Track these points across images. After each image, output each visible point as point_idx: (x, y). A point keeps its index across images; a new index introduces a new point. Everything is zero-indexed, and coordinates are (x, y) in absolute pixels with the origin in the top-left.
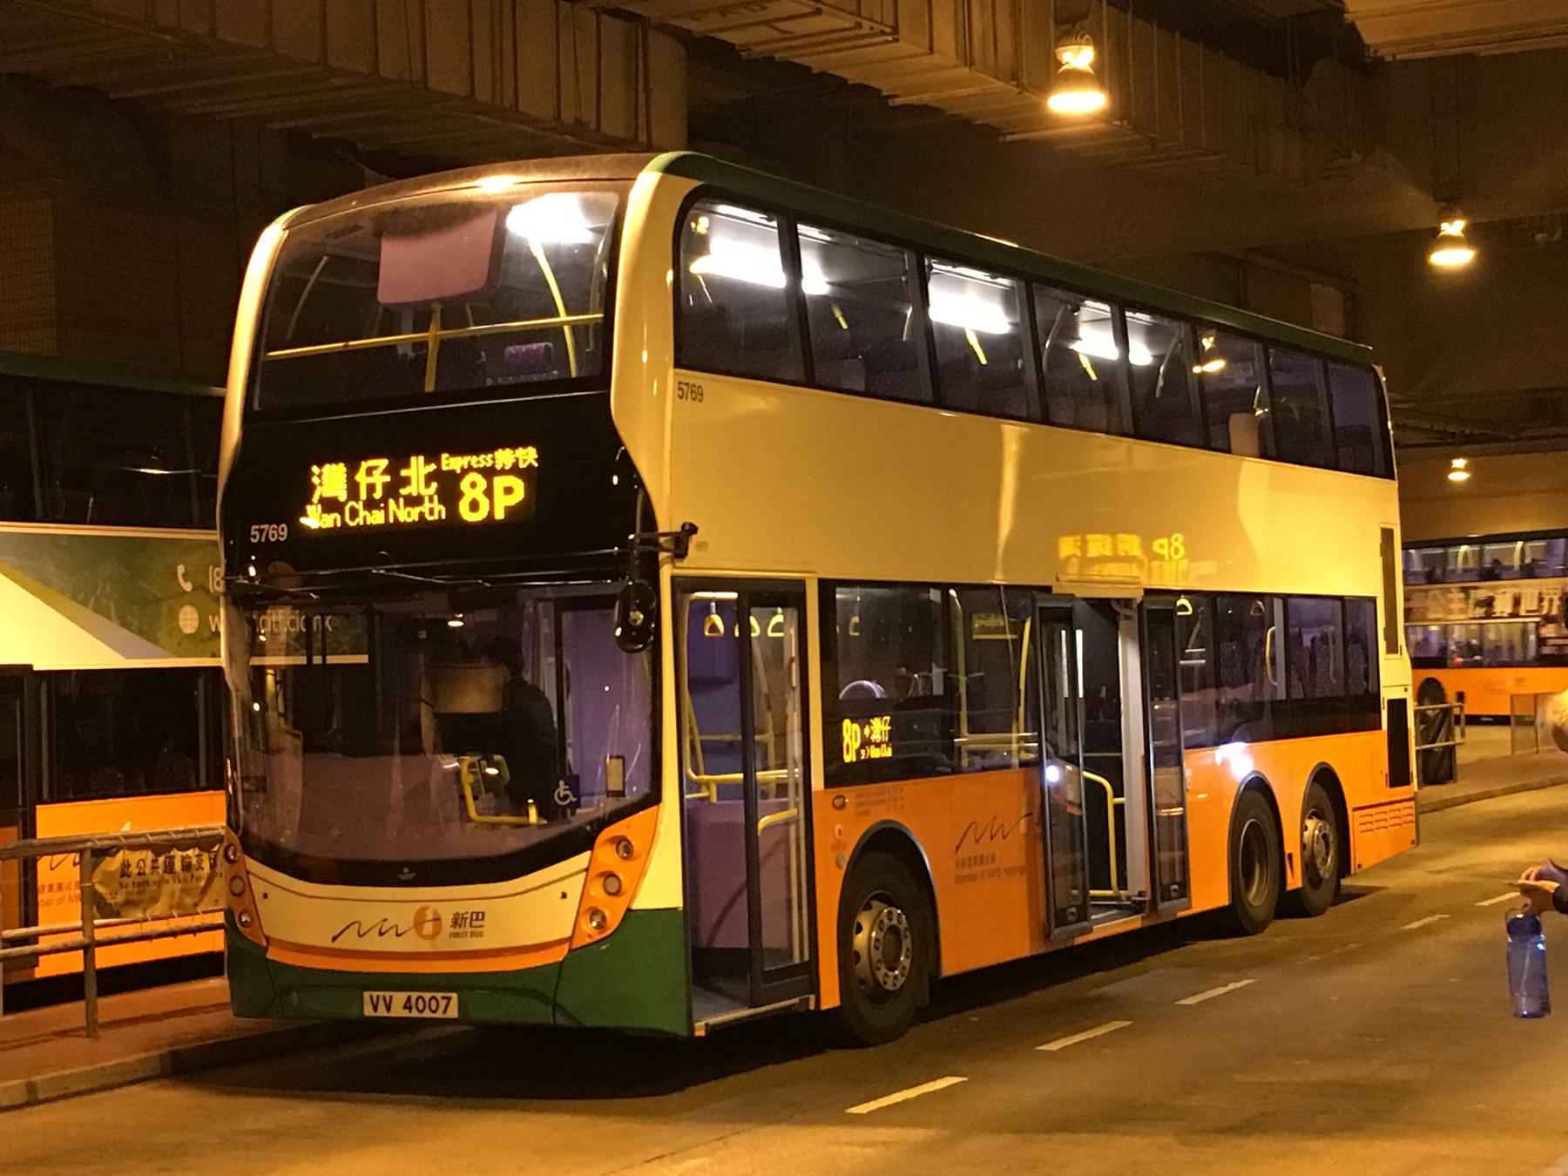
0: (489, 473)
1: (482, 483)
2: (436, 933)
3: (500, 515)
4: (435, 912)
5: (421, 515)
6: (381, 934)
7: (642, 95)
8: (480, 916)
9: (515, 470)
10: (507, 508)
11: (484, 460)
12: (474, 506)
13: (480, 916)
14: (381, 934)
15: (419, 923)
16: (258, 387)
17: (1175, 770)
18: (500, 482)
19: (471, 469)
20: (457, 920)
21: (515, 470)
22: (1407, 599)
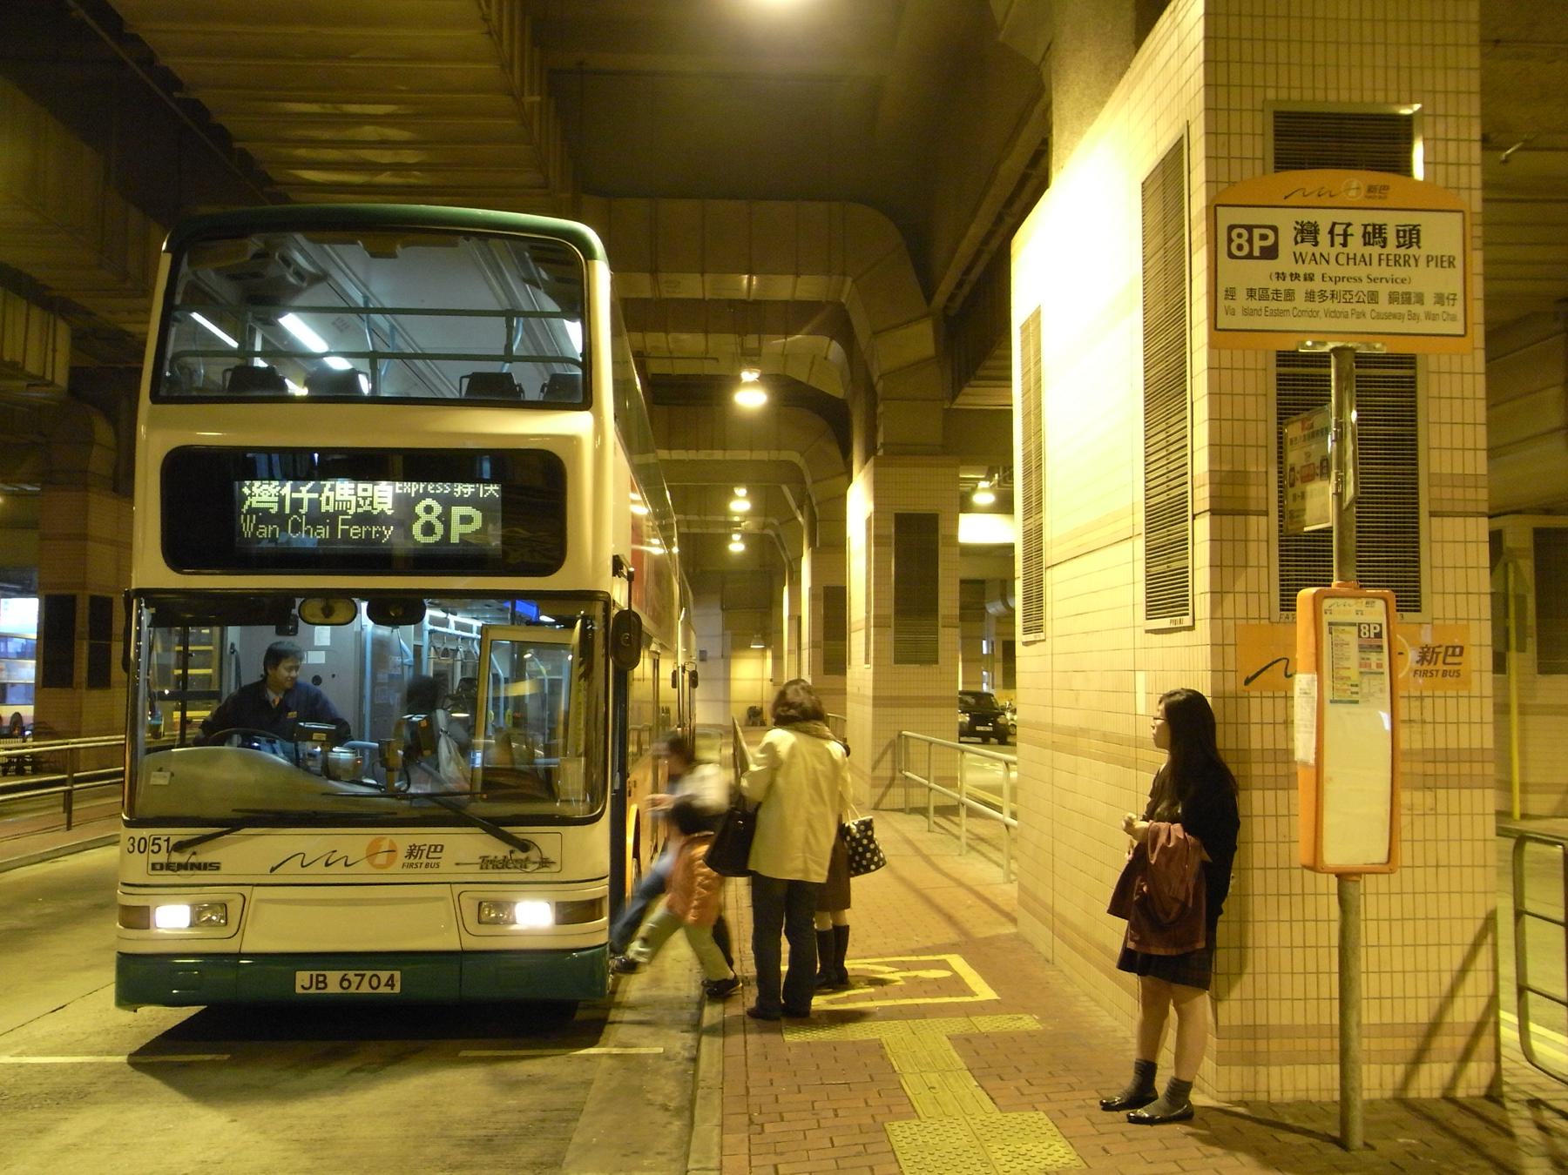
0: (448, 502)
1: (438, 509)
2: (390, 863)
3: (455, 539)
4: (391, 842)
5: (369, 533)
6: (327, 865)
7: (50, 353)
8: (1386, 188)
9: (473, 501)
10: (461, 535)
11: (443, 488)
12: (428, 529)
13: (1386, 188)
14: (327, 865)
15: (371, 855)
16: (249, 394)
17: (1484, 508)
18: (457, 512)
19: (426, 495)
20: (412, 852)
21: (473, 501)
22: (1519, 696)
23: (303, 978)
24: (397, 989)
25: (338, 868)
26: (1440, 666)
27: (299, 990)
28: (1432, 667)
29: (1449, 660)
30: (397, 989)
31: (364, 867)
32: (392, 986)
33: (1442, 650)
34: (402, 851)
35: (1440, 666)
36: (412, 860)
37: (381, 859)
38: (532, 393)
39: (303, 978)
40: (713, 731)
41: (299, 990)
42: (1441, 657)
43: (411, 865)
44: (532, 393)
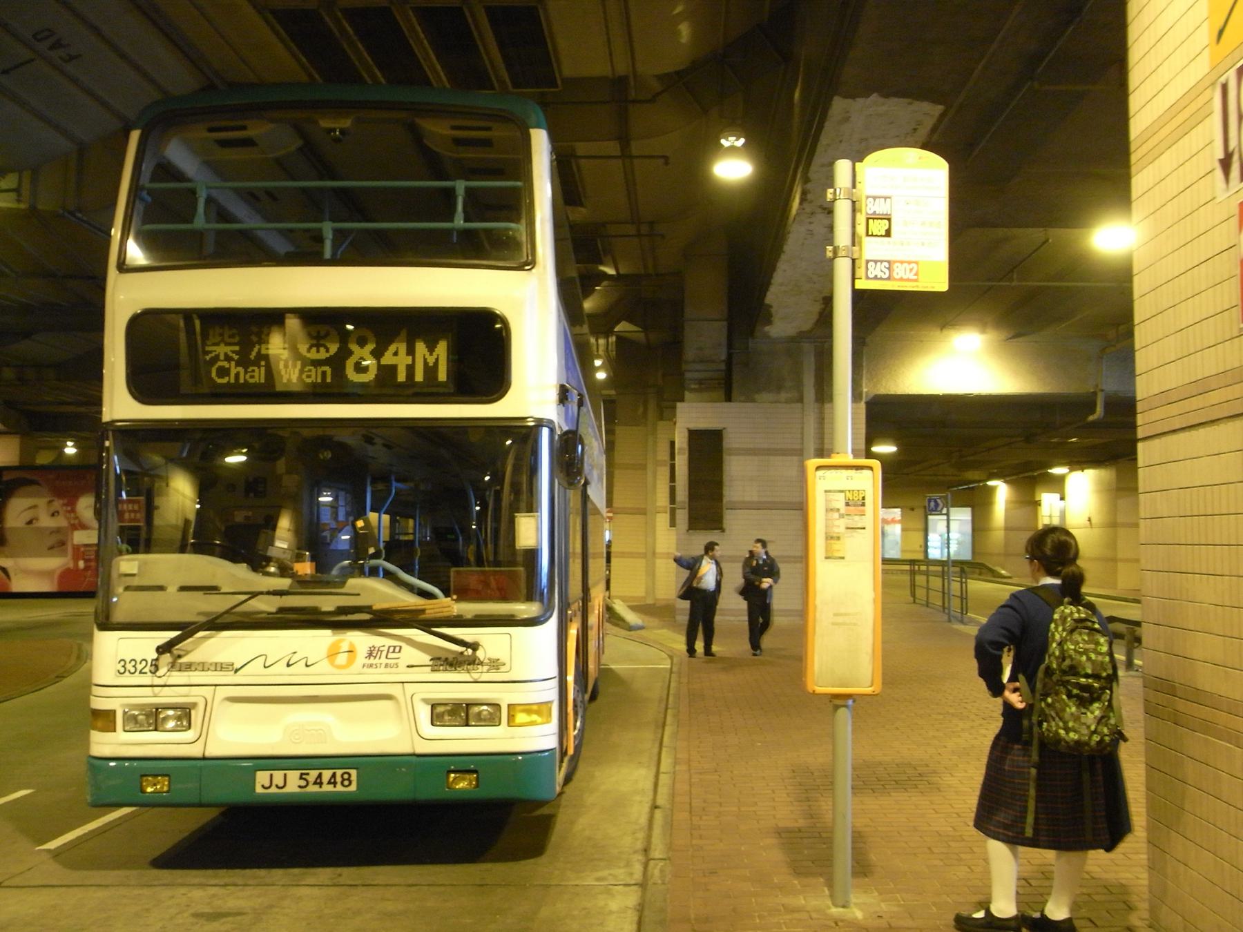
2: (351, 661)
6: (288, 665)
14: (288, 665)
15: (332, 654)
23: (262, 777)
24: (353, 788)
25: (300, 668)
26: (384, 660)
27: (259, 790)
28: (377, 661)
29: (390, 655)
30: (353, 788)
31: (324, 666)
32: (335, 784)
33: (386, 649)
34: (362, 651)
35: (384, 660)
36: (372, 661)
37: (342, 659)
38: (292, 323)
39: (262, 777)
40: (740, 536)
41: (259, 790)
42: (384, 654)
43: (371, 666)
44: (292, 323)
